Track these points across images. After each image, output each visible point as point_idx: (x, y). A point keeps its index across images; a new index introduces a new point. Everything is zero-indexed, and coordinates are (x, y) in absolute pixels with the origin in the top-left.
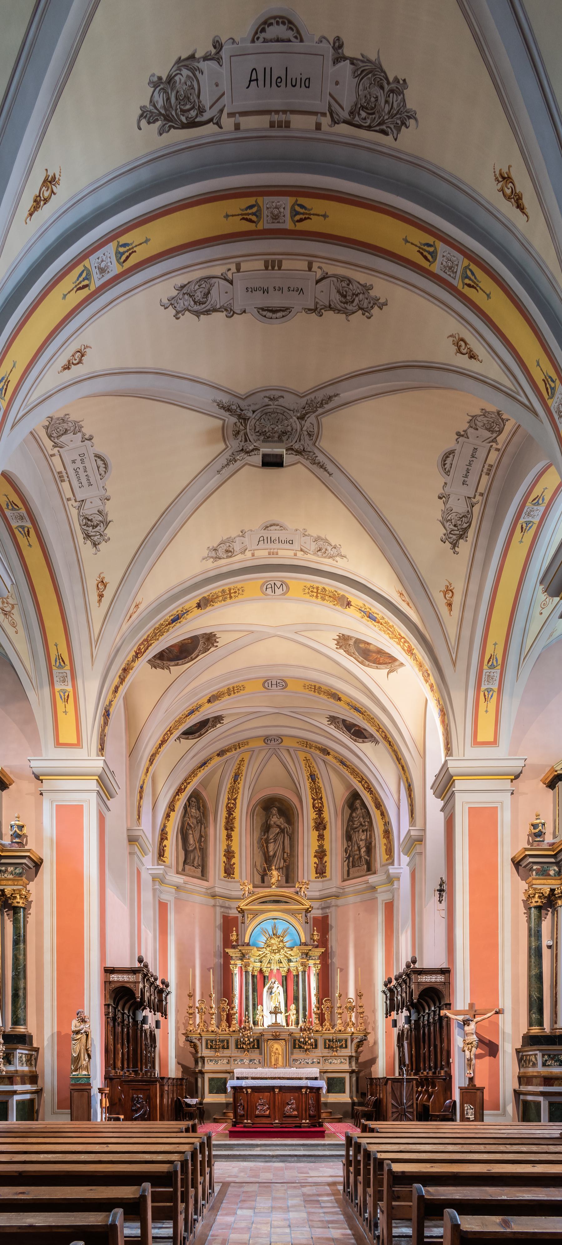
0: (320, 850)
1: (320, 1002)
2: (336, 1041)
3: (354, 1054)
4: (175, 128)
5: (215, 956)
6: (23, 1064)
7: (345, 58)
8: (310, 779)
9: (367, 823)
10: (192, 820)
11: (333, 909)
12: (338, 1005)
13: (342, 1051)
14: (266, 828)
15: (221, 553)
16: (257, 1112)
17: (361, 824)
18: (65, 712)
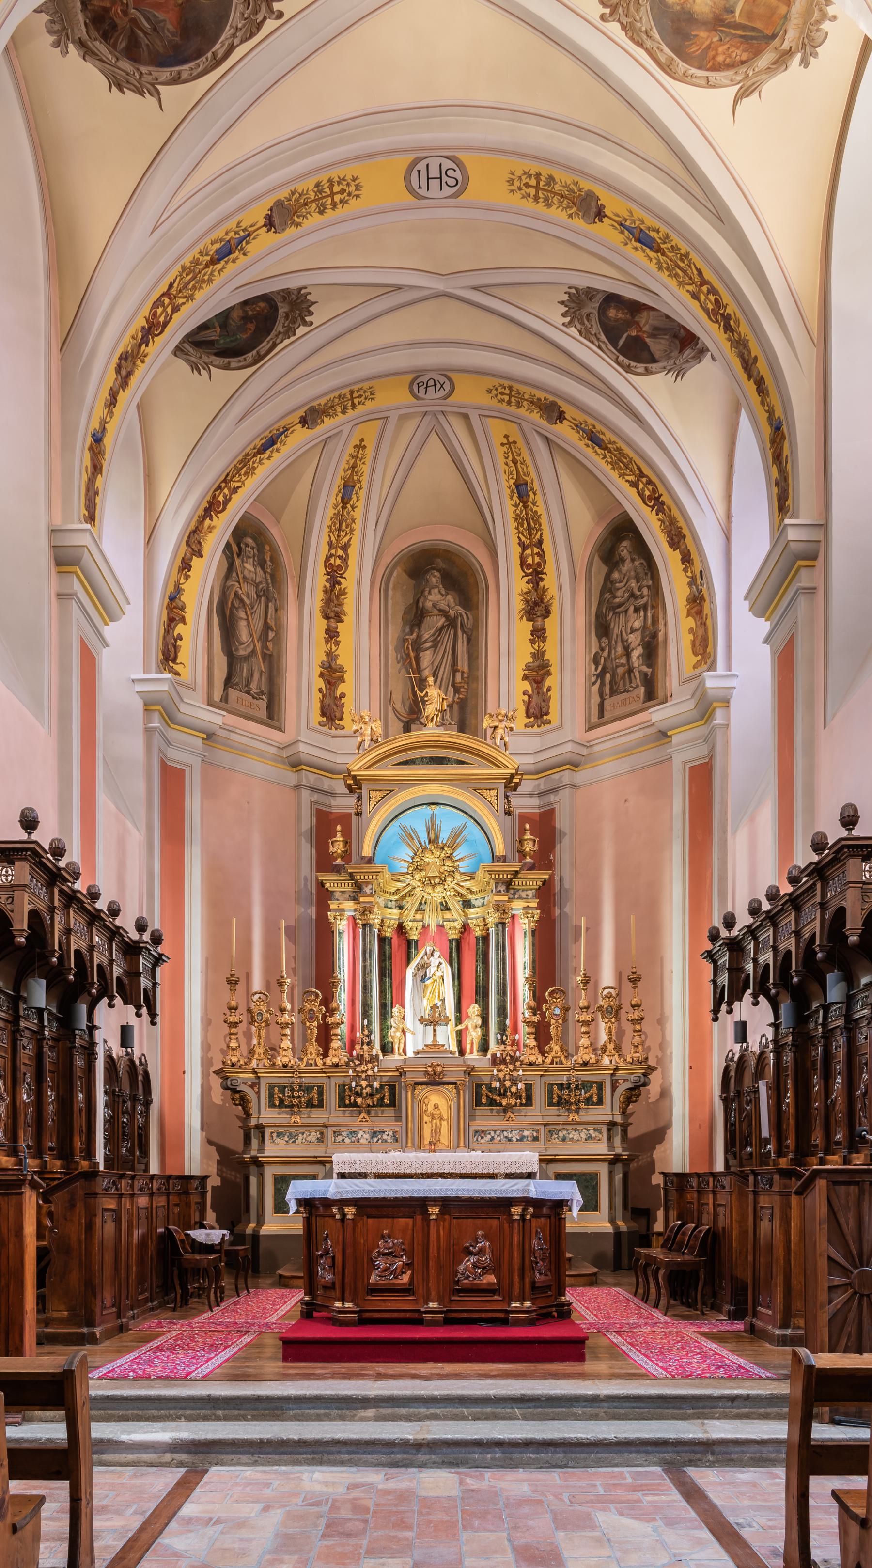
0: (537, 664)
1: (538, 997)
2: (577, 1087)
3: (618, 1119)
5: (297, 900)
8: (516, 496)
9: (645, 591)
10: (245, 587)
11: (565, 794)
12: (583, 1003)
13: (591, 1112)
16: (373, 1278)
17: (632, 595)
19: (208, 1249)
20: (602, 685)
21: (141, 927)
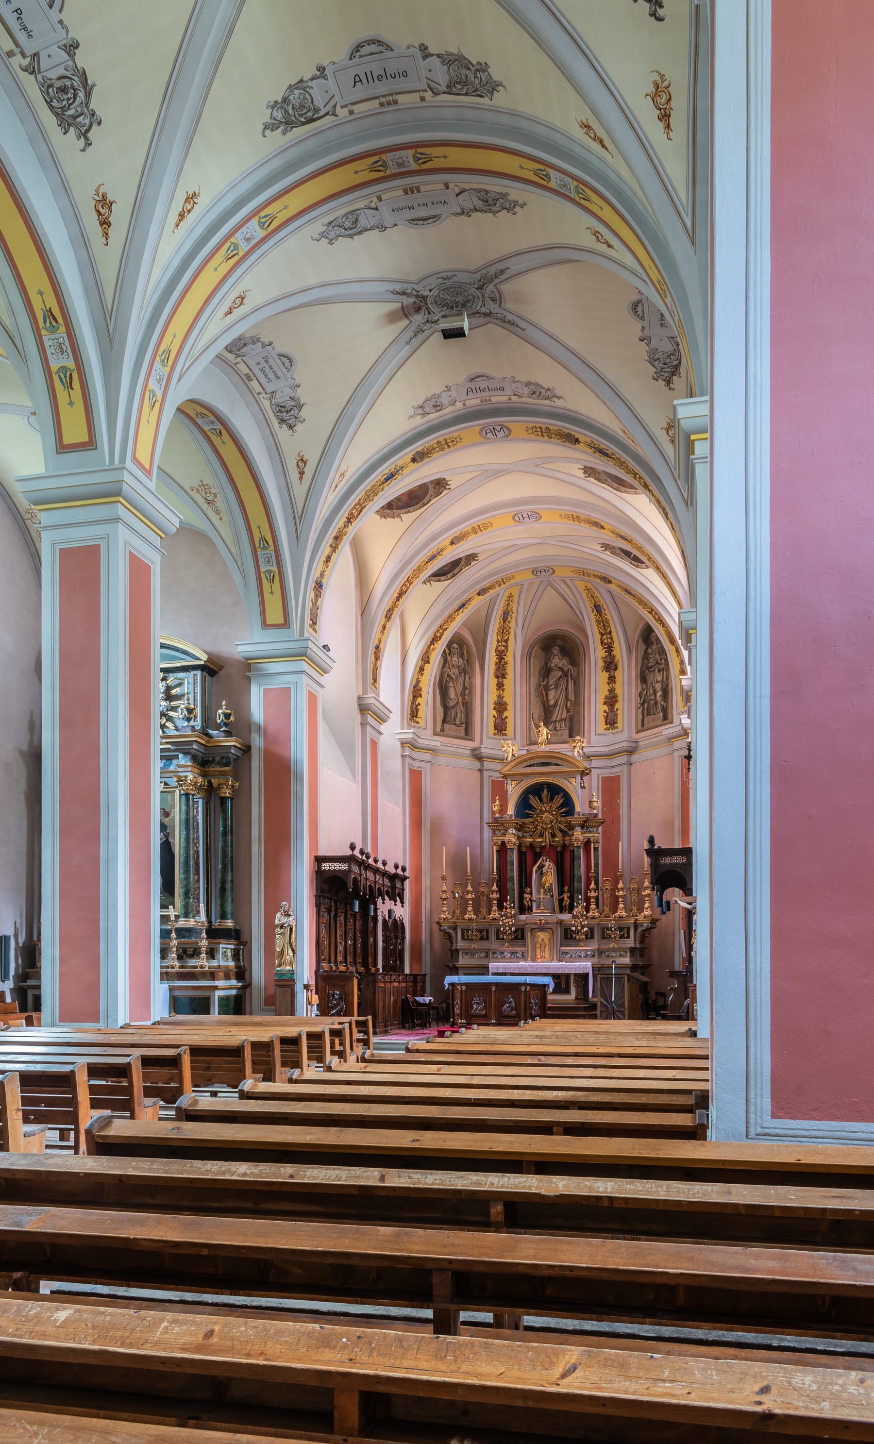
2: (615, 930)
4: (295, 127)
6: (228, 959)
7: (432, 55)
8: (595, 611)
10: (453, 670)
14: (546, 672)
15: (428, 408)
17: (657, 662)
18: (272, 593)
19: (425, 1005)
20: (643, 709)
21: (396, 867)
